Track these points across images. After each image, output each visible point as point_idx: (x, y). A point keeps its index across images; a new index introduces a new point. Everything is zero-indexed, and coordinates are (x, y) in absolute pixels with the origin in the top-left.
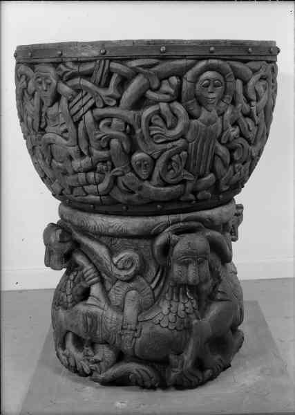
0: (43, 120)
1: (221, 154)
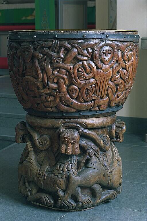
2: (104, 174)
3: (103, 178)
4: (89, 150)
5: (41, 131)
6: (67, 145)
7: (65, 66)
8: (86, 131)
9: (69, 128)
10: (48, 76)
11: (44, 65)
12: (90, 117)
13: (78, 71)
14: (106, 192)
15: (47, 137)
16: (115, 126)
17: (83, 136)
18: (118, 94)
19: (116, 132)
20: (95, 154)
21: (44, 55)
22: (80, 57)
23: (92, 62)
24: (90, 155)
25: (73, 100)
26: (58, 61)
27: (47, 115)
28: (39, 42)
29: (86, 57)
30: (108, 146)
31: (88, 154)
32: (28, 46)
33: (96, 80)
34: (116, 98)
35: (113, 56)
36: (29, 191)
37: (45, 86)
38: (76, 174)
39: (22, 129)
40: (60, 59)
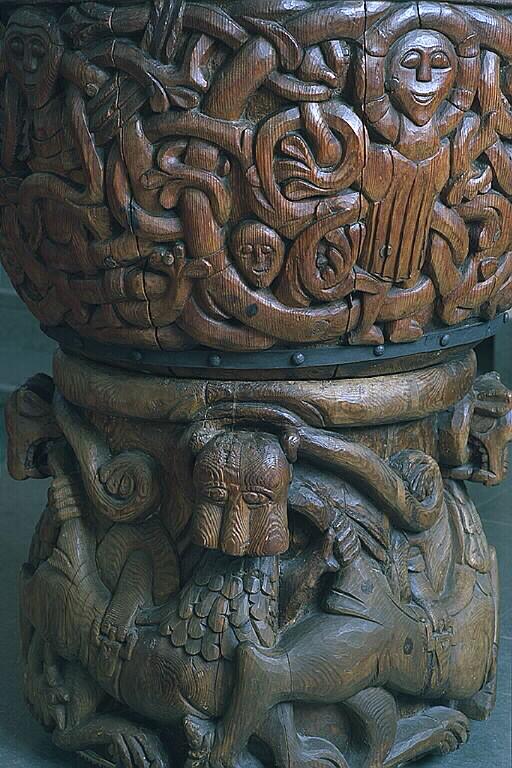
0: (25, 142)
1: (446, 232)
2: (409, 641)
3: (402, 660)
4: (336, 530)
5: (113, 432)
6: (227, 508)
7: (216, 127)
8: (323, 440)
9: (242, 423)
10: (133, 178)
11: (112, 122)
12: (341, 372)
13: (279, 152)
14: (419, 715)
15: (138, 462)
16: (466, 409)
17: (308, 461)
18: (480, 266)
19: (473, 441)
20: (364, 547)
21: (111, 71)
22: (291, 86)
23: (350, 111)
24: (338, 556)
25: (255, 295)
26: (180, 102)
27: (135, 363)
28: (87, 6)
29: (322, 82)
30: (427, 507)
31: (330, 547)
32: (36, 30)
33: (370, 201)
34: (468, 287)
35: (458, 80)
36: (62, 702)
37: (121, 225)
38: (269, 640)
39: (37, 414)
40: (189, 93)
